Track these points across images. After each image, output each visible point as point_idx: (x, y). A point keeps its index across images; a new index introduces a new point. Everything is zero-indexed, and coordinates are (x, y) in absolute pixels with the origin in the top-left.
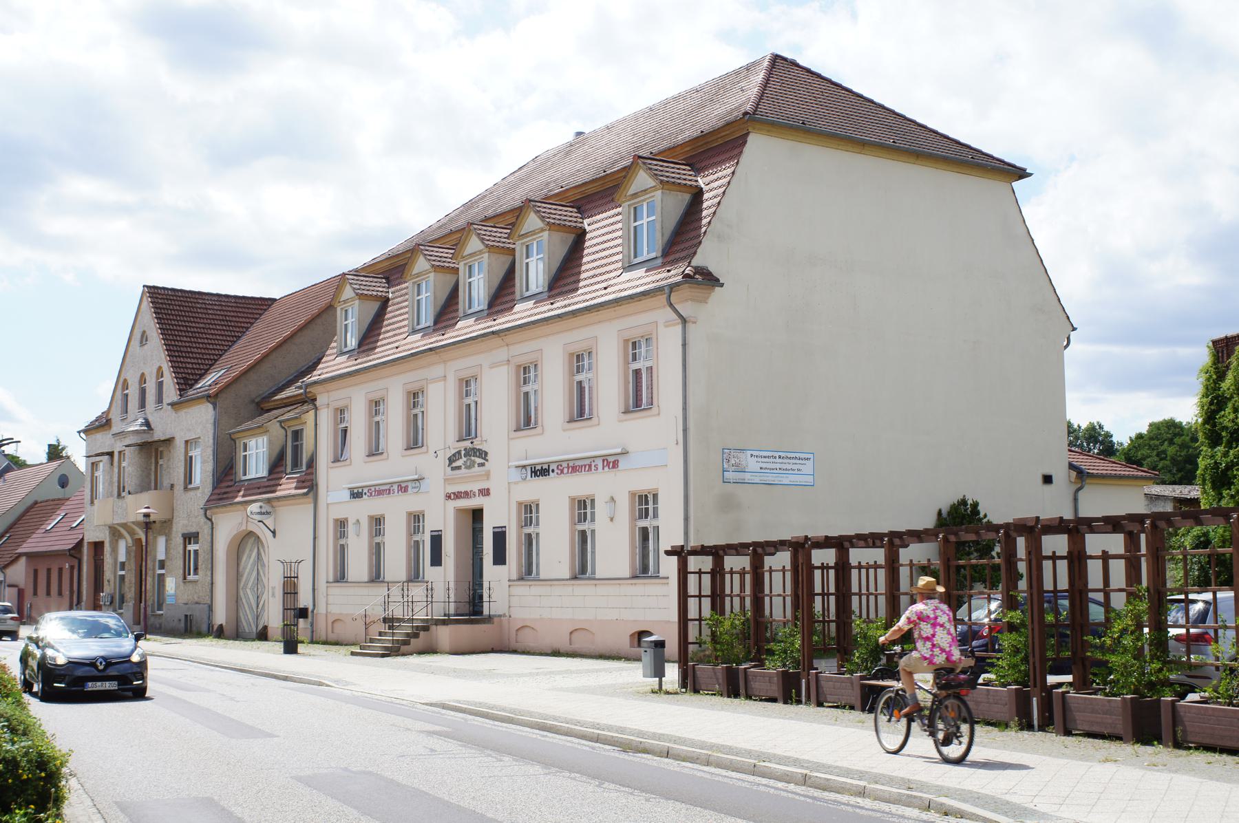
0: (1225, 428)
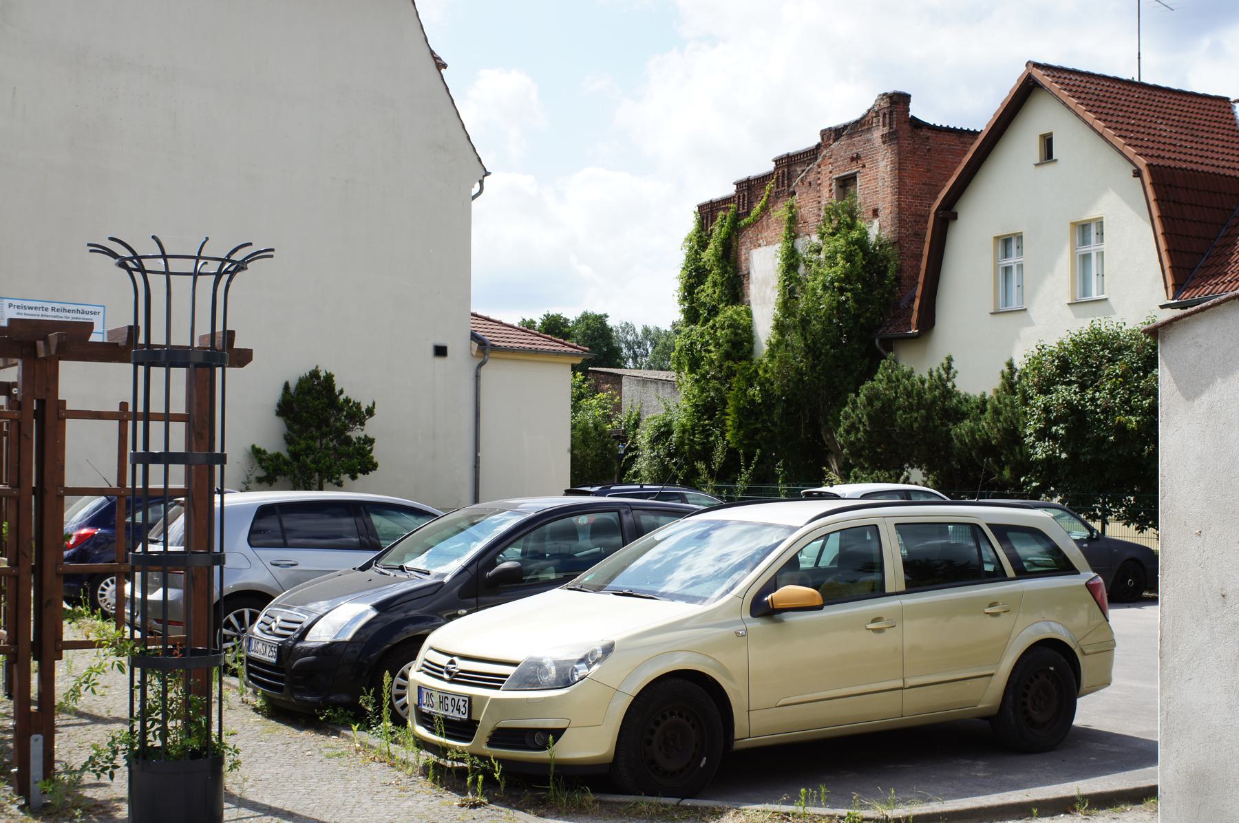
0: (704, 304)
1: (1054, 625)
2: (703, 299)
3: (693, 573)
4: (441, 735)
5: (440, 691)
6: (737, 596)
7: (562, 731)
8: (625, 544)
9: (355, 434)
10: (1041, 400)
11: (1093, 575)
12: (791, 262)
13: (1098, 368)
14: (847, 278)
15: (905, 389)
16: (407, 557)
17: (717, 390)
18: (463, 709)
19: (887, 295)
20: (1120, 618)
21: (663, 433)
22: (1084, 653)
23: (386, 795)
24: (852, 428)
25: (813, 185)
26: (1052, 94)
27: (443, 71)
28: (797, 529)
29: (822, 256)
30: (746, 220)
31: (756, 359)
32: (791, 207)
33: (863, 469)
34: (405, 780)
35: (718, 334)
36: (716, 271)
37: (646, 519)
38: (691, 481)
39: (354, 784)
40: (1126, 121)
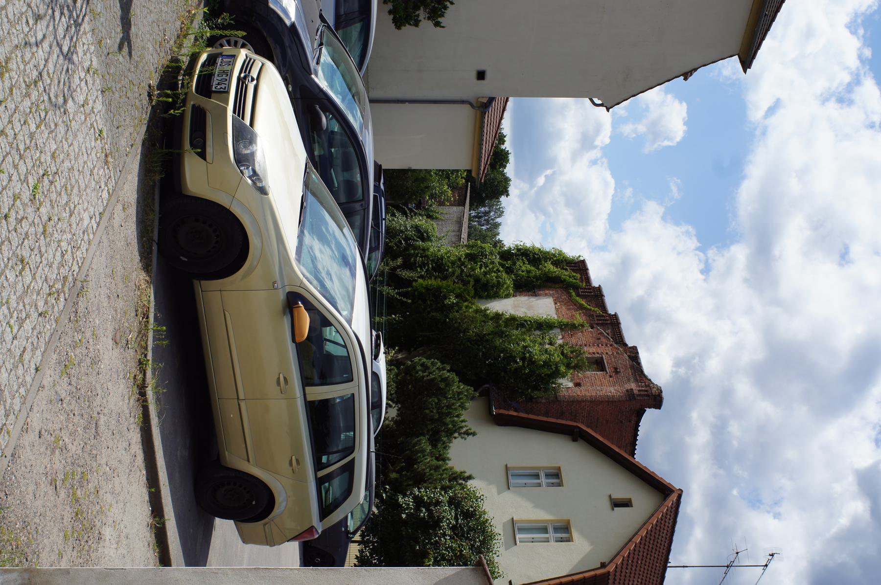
0: (515, 264)
1: (284, 504)
2: (518, 263)
3: (318, 254)
4: (200, 71)
5: (232, 71)
6: (302, 282)
7: (205, 159)
8: (340, 204)
9: (422, 14)
10: (444, 498)
11: (320, 531)
12: (543, 326)
13: (467, 538)
14: (532, 362)
15: (453, 404)
16: (330, 48)
17: (453, 273)
18: (219, 87)
19: (518, 390)
20: (292, 550)
21: (422, 234)
22: (265, 525)
23: (157, 31)
24: (425, 367)
25: (597, 342)
26: (659, 507)
27: (682, 78)
28: (350, 325)
29: (547, 346)
30: (574, 294)
31: (475, 301)
32: (582, 326)
33: (397, 375)
34: (168, 46)
35: (493, 274)
36: (538, 273)
37: (358, 219)
38: (389, 253)
39: (165, 9)
40: (640, 558)
